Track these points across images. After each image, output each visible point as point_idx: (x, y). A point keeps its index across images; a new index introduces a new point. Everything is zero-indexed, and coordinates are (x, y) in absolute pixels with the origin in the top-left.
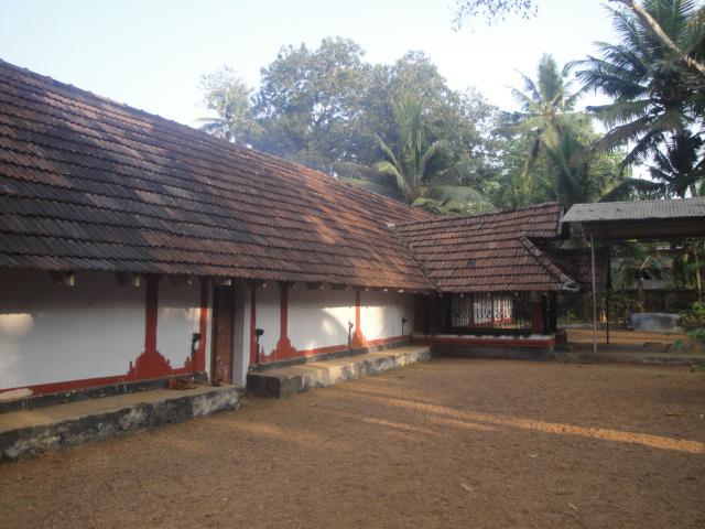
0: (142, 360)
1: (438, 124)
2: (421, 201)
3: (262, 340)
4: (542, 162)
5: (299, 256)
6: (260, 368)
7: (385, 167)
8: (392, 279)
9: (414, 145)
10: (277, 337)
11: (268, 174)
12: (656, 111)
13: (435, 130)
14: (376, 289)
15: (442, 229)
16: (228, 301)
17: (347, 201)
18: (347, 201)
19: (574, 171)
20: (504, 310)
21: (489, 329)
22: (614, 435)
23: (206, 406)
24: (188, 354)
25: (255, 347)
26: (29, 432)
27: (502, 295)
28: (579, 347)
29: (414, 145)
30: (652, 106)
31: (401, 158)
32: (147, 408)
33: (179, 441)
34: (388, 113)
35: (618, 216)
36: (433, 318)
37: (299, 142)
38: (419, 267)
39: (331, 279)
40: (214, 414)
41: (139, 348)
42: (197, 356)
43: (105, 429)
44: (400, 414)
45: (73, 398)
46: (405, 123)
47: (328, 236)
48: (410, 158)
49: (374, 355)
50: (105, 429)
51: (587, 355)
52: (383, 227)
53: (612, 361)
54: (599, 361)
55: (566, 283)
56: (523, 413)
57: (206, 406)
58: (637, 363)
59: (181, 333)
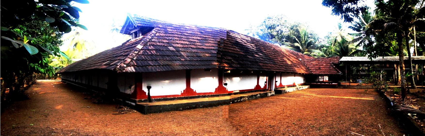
0: (256, 86)
1: (311, 34)
2: (305, 53)
3: (277, 83)
4: (337, 44)
5: (284, 67)
6: (277, 88)
7: (296, 44)
8: (302, 71)
9: (305, 39)
10: (280, 83)
11: (274, 49)
12: (364, 35)
13: (309, 36)
14: (299, 73)
15: (313, 61)
16: (271, 76)
17: (290, 54)
18: (290, 54)
19: (344, 47)
20: (326, 78)
21: (323, 82)
22: (346, 97)
23: (270, 94)
24: (264, 85)
25: (276, 84)
26: (244, 97)
27: (326, 75)
28: (342, 86)
29: (305, 39)
30: (363, 34)
31: (301, 42)
32: (260, 94)
33: (265, 100)
34: (297, 31)
35: (351, 60)
36: (311, 80)
37: (273, 37)
38: (308, 69)
39: (292, 71)
40: (271, 96)
41: (256, 84)
42: (266, 85)
43: (254, 97)
44: (307, 95)
45: (246, 93)
46: (302, 35)
47: (289, 63)
48: (303, 42)
49: (298, 87)
50: (254, 97)
51: (344, 87)
52: (299, 60)
53: (350, 88)
54: (347, 88)
55: (340, 73)
56: (331, 95)
57: (270, 94)
58: (355, 88)
59: (263, 81)
